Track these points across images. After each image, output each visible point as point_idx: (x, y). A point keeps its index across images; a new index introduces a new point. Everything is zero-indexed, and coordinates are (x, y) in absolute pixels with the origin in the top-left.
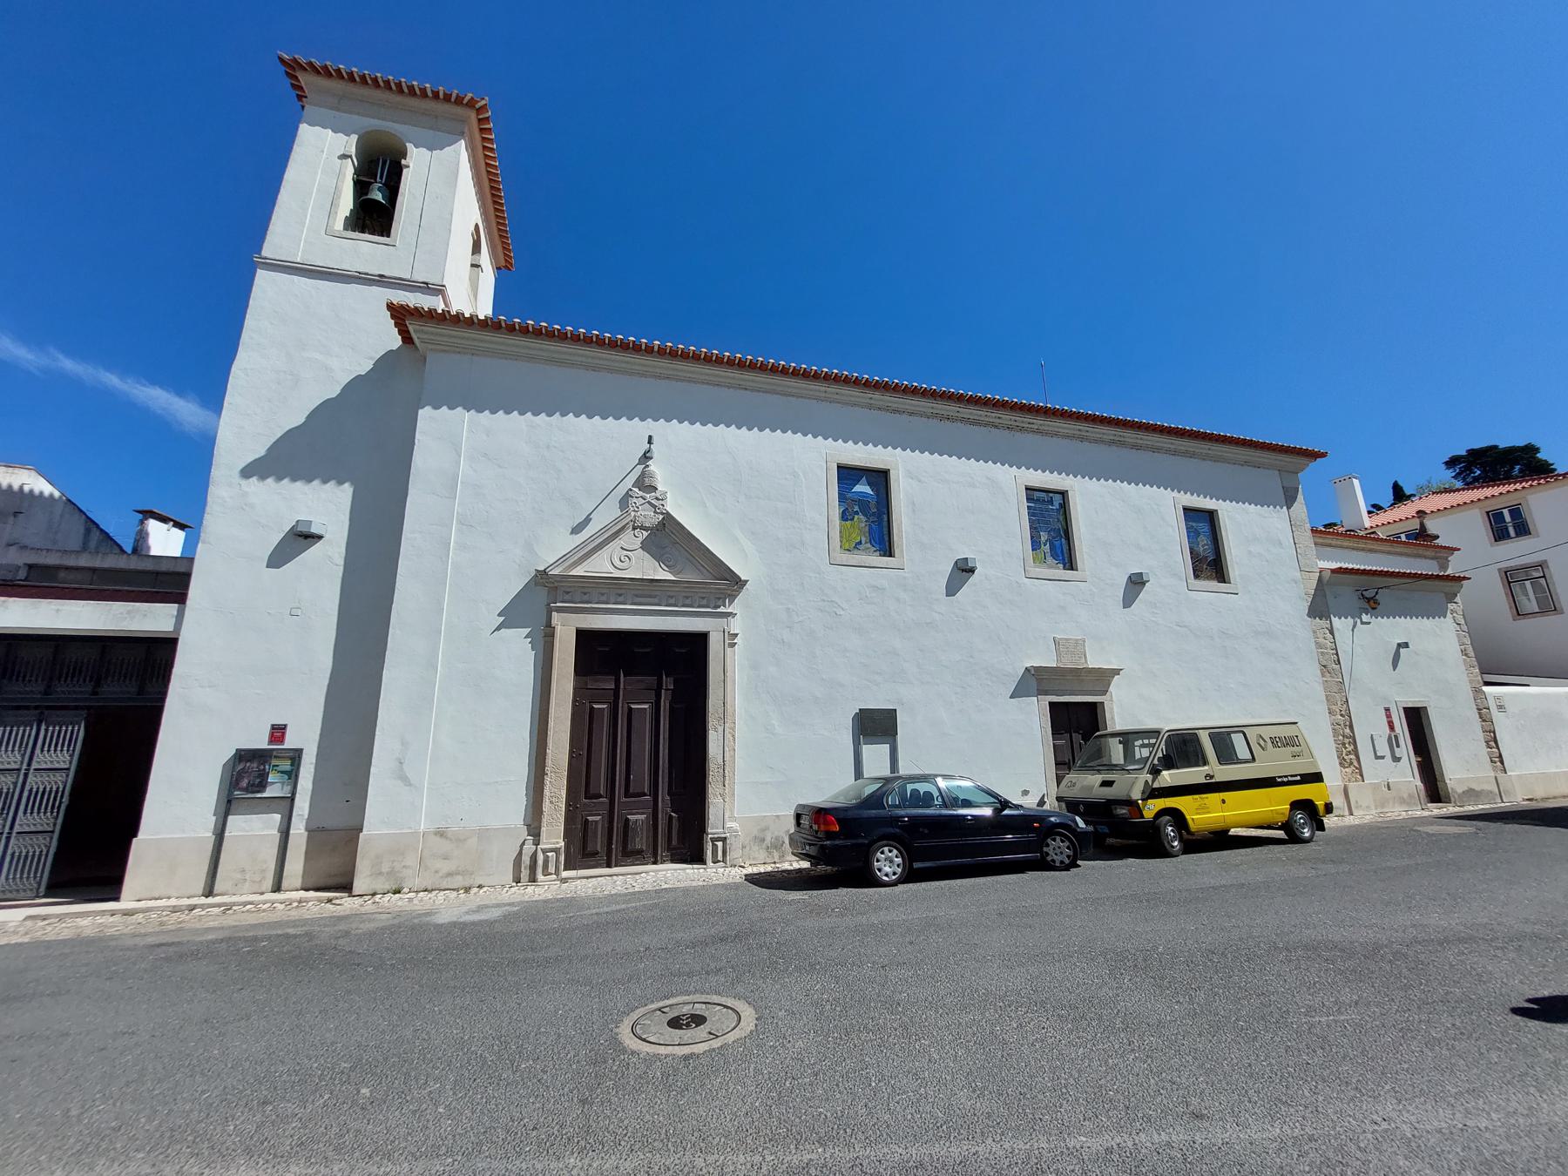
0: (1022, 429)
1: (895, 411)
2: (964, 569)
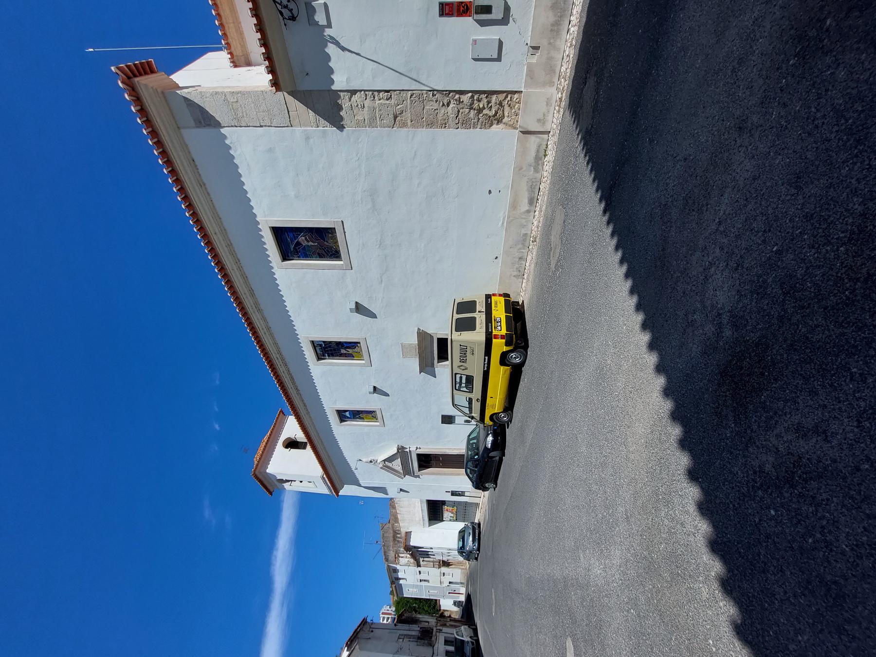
0: (283, 359)
1: (305, 405)
2: (359, 308)
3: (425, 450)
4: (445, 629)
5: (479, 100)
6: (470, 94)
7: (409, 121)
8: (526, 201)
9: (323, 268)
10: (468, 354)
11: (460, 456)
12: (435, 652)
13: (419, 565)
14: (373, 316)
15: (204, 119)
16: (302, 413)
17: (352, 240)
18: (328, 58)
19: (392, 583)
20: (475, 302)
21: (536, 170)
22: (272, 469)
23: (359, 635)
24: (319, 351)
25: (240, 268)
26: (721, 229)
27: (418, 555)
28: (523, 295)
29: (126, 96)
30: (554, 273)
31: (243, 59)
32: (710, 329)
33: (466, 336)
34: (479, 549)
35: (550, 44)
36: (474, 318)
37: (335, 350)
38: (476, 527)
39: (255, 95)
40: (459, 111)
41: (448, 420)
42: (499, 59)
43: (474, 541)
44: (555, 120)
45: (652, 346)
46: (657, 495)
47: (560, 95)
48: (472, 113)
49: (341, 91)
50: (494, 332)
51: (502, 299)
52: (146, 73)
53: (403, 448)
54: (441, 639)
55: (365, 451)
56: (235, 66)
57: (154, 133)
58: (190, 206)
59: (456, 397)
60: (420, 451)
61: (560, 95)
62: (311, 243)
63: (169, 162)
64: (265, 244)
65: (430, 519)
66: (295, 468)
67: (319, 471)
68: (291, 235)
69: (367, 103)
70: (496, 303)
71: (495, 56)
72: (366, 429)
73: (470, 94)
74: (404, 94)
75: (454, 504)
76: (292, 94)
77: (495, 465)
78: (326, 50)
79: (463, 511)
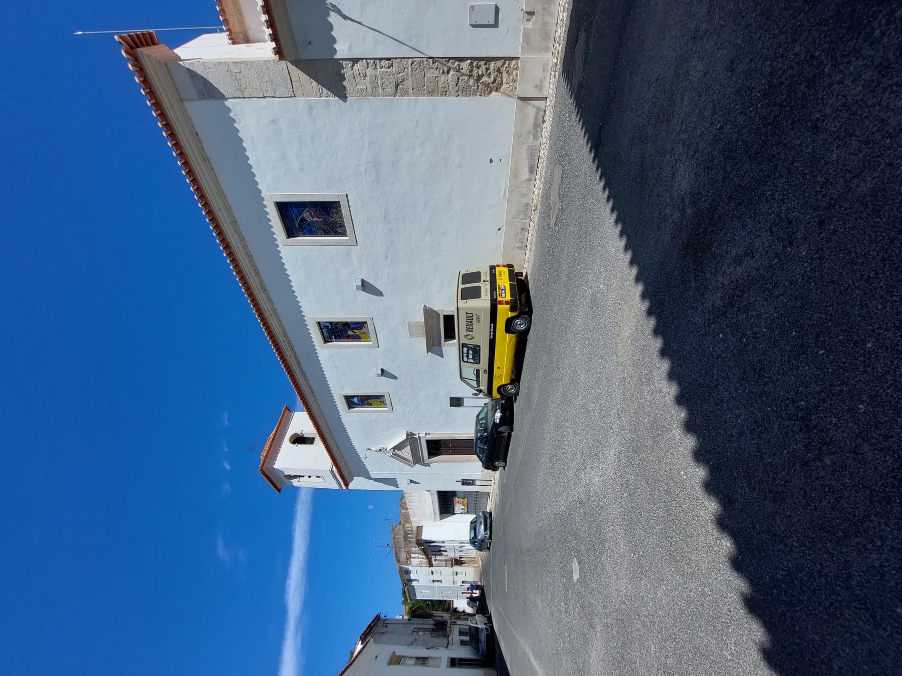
0: (289, 343)
1: (312, 392)
2: (365, 286)
3: (435, 435)
4: (459, 622)
5: (478, 67)
6: (469, 61)
7: (410, 89)
8: (526, 169)
9: (329, 244)
10: (474, 322)
11: (470, 441)
12: (450, 642)
13: (431, 565)
14: (379, 293)
15: (206, 90)
16: (310, 400)
17: (356, 215)
18: (331, 27)
19: (405, 584)
20: (480, 273)
21: (536, 138)
22: (279, 464)
23: (375, 629)
24: (325, 334)
25: (245, 247)
26: (683, 127)
27: (431, 550)
28: (526, 266)
29: (130, 66)
30: (554, 231)
31: (241, 36)
32: (677, 215)
33: (472, 303)
34: (490, 538)
35: (544, 9)
36: (480, 287)
37: (341, 331)
38: (488, 516)
39: (258, 65)
40: (459, 79)
41: (456, 402)
42: (496, 25)
43: (485, 529)
44: (551, 86)
45: (680, 400)
46: (641, 380)
47: (555, 60)
48: (471, 82)
49: (342, 60)
50: (499, 299)
51: (506, 269)
52: (148, 45)
53: (412, 434)
54: (456, 630)
55: (372, 437)
56: (234, 43)
57: (158, 105)
58: (194, 181)
59: (463, 369)
60: (429, 437)
61: (555, 60)
62: (316, 219)
63: (172, 135)
64: (270, 220)
65: (441, 513)
66: (304, 463)
67: (329, 462)
68: (295, 210)
69: (369, 71)
70: (500, 273)
71: (492, 22)
72: (375, 415)
73: (469, 61)
74: (404, 62)
75: (466, 494)
76: (297, 63)
77: (505, 440)
78: (329, 19)
79: (474, 501)
